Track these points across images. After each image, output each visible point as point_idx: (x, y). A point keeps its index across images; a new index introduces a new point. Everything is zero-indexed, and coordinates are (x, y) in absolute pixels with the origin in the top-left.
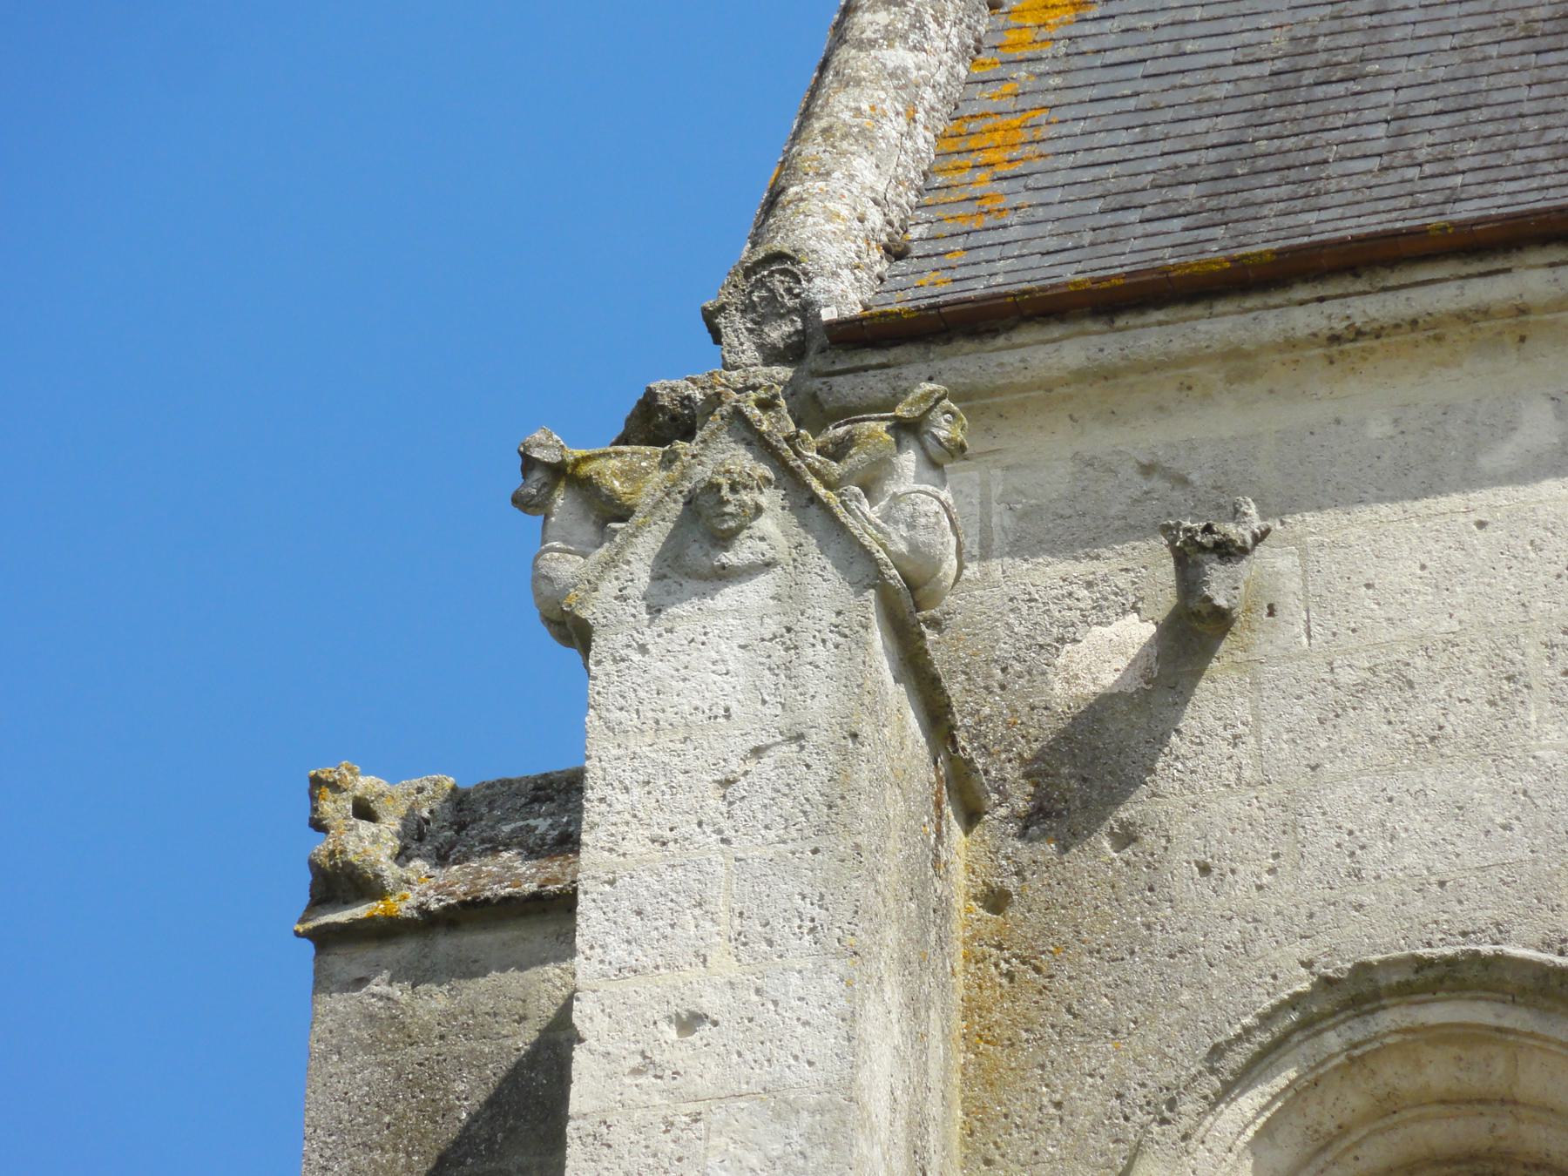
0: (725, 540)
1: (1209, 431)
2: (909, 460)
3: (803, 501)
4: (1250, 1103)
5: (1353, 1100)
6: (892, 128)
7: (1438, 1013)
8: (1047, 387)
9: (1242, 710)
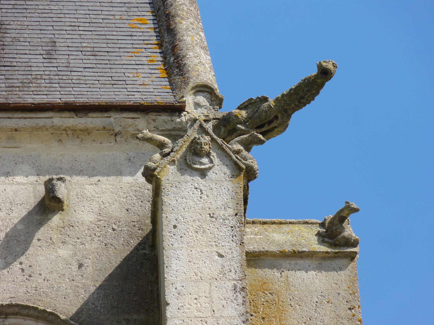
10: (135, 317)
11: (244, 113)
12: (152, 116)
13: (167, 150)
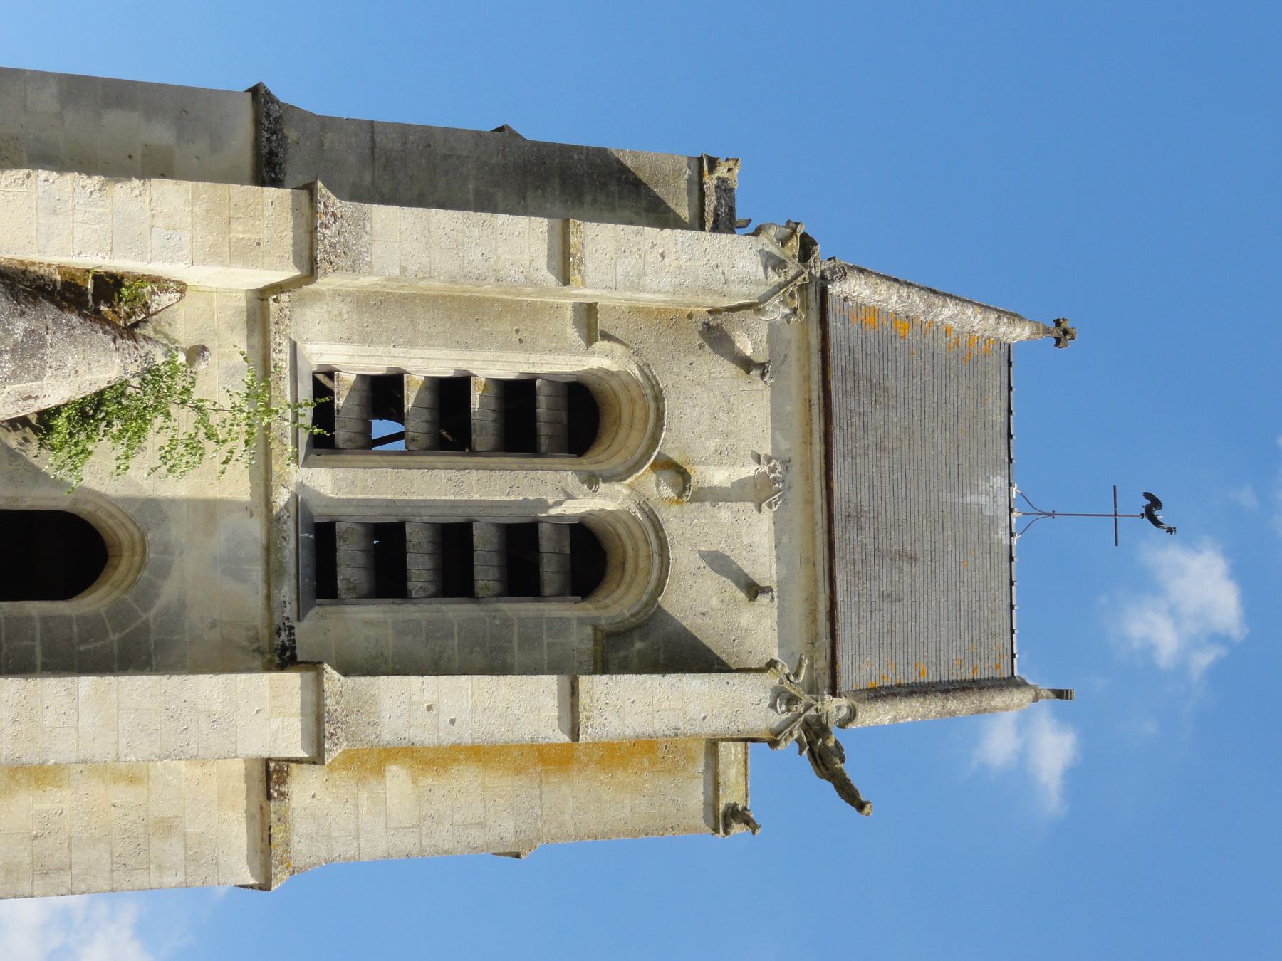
0: (774, 268)
1: (793, 371)
2: (787, 311)
3: (781, 286)
4: (636, 372)
5: (635, 393)
6: (877, 298)
7: (652, 416)
8: (807, 335)
9: (728, 374)
10: (662, 657)
11: (831, 744)
12: (828, 672)
13: (792, 678)
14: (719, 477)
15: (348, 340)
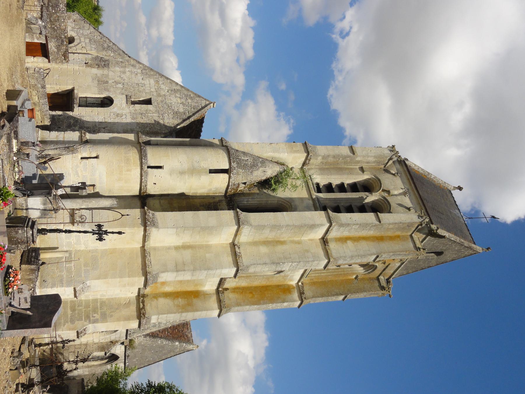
14: (396, 193)
15: (319, 175)
